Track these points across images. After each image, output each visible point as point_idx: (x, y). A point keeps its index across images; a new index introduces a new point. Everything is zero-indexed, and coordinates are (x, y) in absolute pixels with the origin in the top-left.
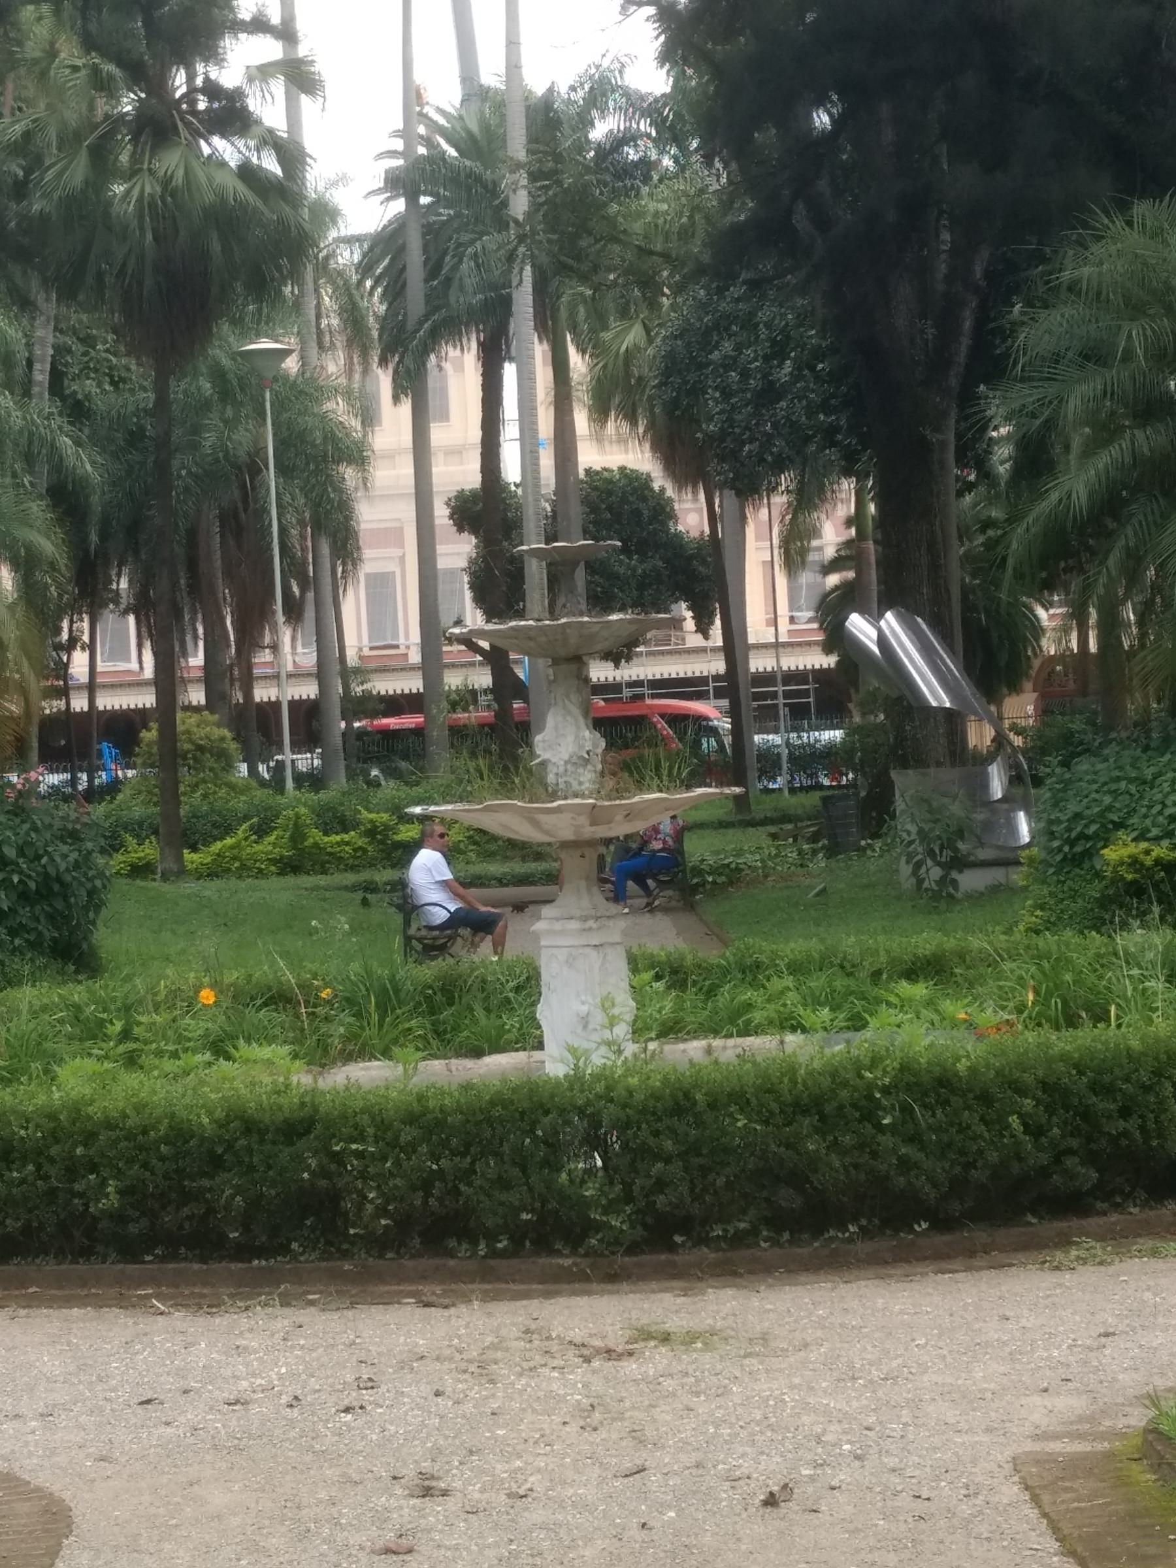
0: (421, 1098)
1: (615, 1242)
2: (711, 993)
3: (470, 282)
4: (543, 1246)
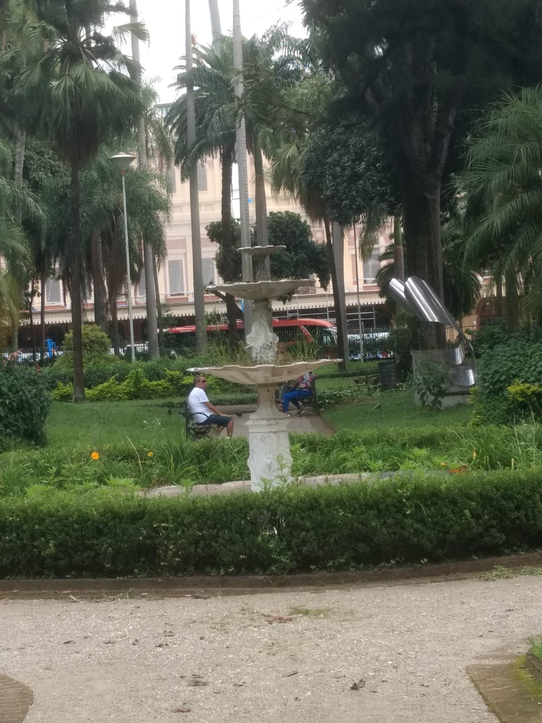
0: (194, 502)
1: (283, 569)
2: (328, 453)
3: (217, 126)
4: (250, 570)
